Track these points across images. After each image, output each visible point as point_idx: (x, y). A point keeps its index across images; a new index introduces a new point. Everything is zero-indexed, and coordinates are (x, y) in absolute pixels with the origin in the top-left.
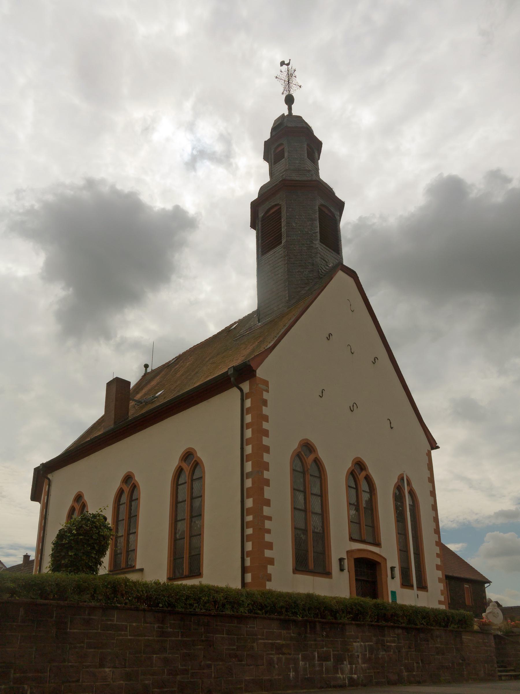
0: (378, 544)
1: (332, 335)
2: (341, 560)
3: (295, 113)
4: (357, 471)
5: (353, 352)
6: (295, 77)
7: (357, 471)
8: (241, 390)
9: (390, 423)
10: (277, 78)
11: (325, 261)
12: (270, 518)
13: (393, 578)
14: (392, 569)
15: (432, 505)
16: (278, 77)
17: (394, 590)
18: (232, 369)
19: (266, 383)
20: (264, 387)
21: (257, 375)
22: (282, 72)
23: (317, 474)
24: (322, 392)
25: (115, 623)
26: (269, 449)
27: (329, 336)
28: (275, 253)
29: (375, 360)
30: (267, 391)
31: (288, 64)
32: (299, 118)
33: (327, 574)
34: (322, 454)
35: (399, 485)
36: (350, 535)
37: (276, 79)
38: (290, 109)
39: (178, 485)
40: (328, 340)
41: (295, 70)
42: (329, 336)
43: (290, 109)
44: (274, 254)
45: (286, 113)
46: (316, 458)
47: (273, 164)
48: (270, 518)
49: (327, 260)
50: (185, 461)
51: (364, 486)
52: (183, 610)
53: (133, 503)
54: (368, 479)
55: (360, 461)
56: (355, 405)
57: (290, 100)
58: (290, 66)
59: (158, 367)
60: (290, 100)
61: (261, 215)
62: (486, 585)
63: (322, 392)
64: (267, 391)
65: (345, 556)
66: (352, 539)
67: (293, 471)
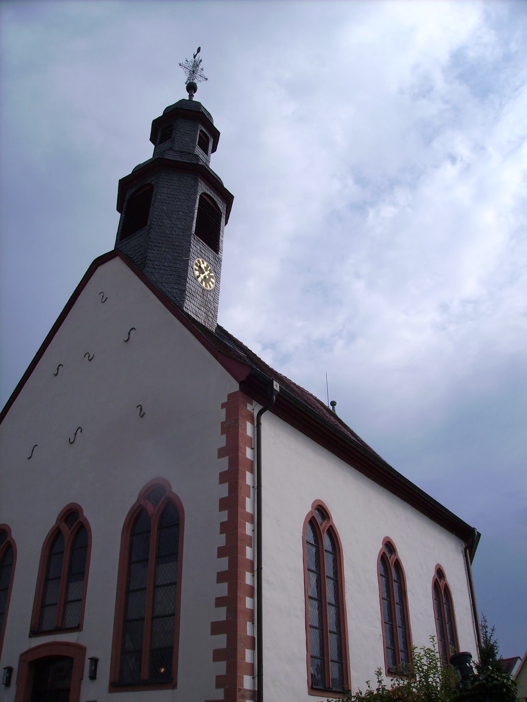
3: (195, 99)
4: (319, 520)
6: (202, 69)
7: (319, 520)
10: (206, 79)
22: (187, 61)
32: (198, 104)
38: (191, 96)
41: (201, 61)
43: (191, 96)
45: (187, 98)
51: (327, 543)
52: (388, 470)
54: (332, 533)
57: (191, 88)
60: (191, 88)
61: (127, 197)
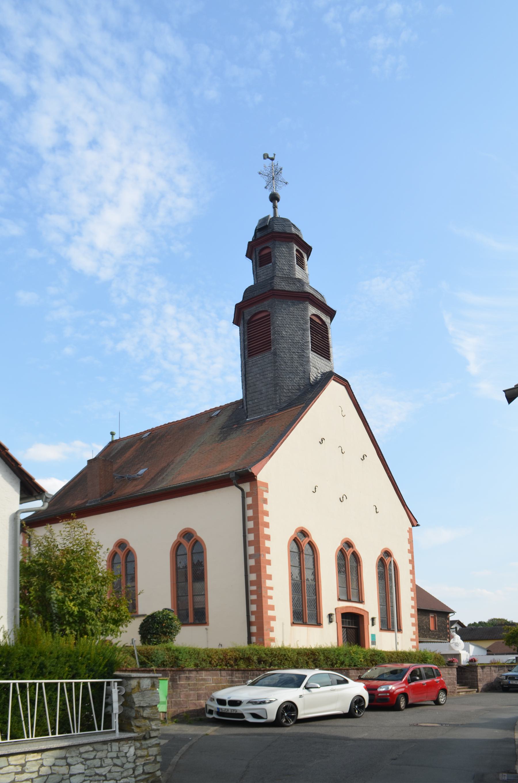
0: (361, 601)
1: (324, 439)
2: (330, 615)
3: (281, 213)
5: (343, 452)
8: (242, 490)
9: (376, 509)
10: (260, 173)
11: (317, 369)
12: (271, 588)
13: (373, 625)
14: (373, 619)
15: (410, 570)
16: (261, 172)
17: (373, 633)
18: (234, 474)
19: (266, 485)
20: (265, 489)
21: (258, 479)
23: (311, 553)
24: (315, 489)
25: (204, 677)
26: (270, 537)
27: (322, 441)
28: (264, 357)
29: (364, 457)
30: (267, 492)
31: (272, 159)
32: (285, 221)
33: (319, 624)
34: (315, 538)
35: (382, 557)
36: (338, 597)
37: (260, 175)
39: (177, 555)
40: (321, 443)
41: (281, 169)
42: (322, 441)
44: (262, 358)
46: (310, 541)
47: (258, 265)
48: (271, 588)
49: (318, 368)
50: (184, 537)
53: (129, 564)
55: (348, 541)
56: (344, 496)
58: (275, 162)
59: (127, 437)
60: (274, 198)
62: (450, 615)
63: (315, 489)
64: (267, 492)
65: (333, 612)
66: (339, 600)
67: (291, 552)
